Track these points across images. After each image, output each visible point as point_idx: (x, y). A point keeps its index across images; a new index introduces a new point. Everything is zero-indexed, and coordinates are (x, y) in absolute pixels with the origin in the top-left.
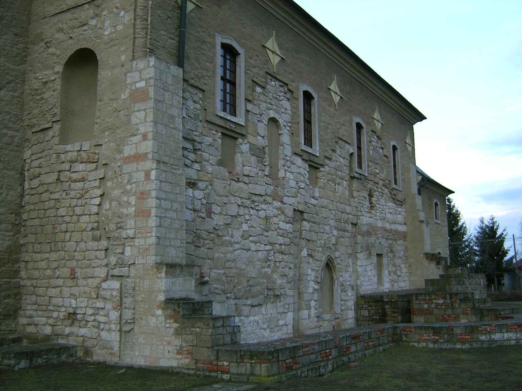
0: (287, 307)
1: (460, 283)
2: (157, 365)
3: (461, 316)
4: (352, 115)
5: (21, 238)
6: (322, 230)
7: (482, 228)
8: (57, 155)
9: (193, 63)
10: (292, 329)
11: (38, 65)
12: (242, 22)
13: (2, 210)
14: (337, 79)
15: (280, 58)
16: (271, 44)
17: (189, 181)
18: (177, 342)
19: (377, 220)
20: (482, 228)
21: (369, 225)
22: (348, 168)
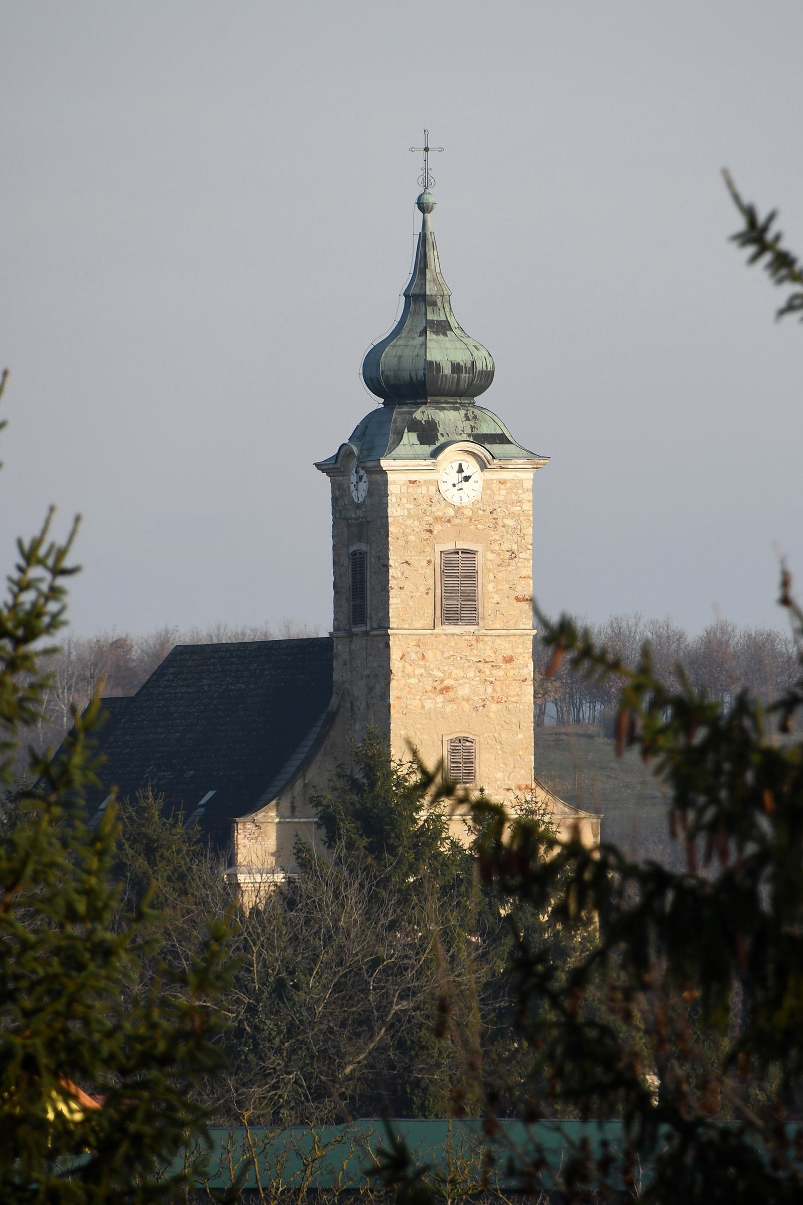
0: (215, 696)
1: (735, 636)
2: (170, 651)
3: (523, 787)
4: (624, 636)
5: (122, 1080)
6: (544, 806)
7: (167, 632)
8: (429, 305)
9: (320, 883)
10: (441, 779)
11: (58, 1168)
12: (342, 889)
13: (201, 1204)
14: (77, 1084)
15: (426, 214)
16: (56, 872)
17: (438, 621)
18: (739, 632)
19: (363, 761)
20: (167, 632)
21: (604, 1117)
22: (454, 387)
